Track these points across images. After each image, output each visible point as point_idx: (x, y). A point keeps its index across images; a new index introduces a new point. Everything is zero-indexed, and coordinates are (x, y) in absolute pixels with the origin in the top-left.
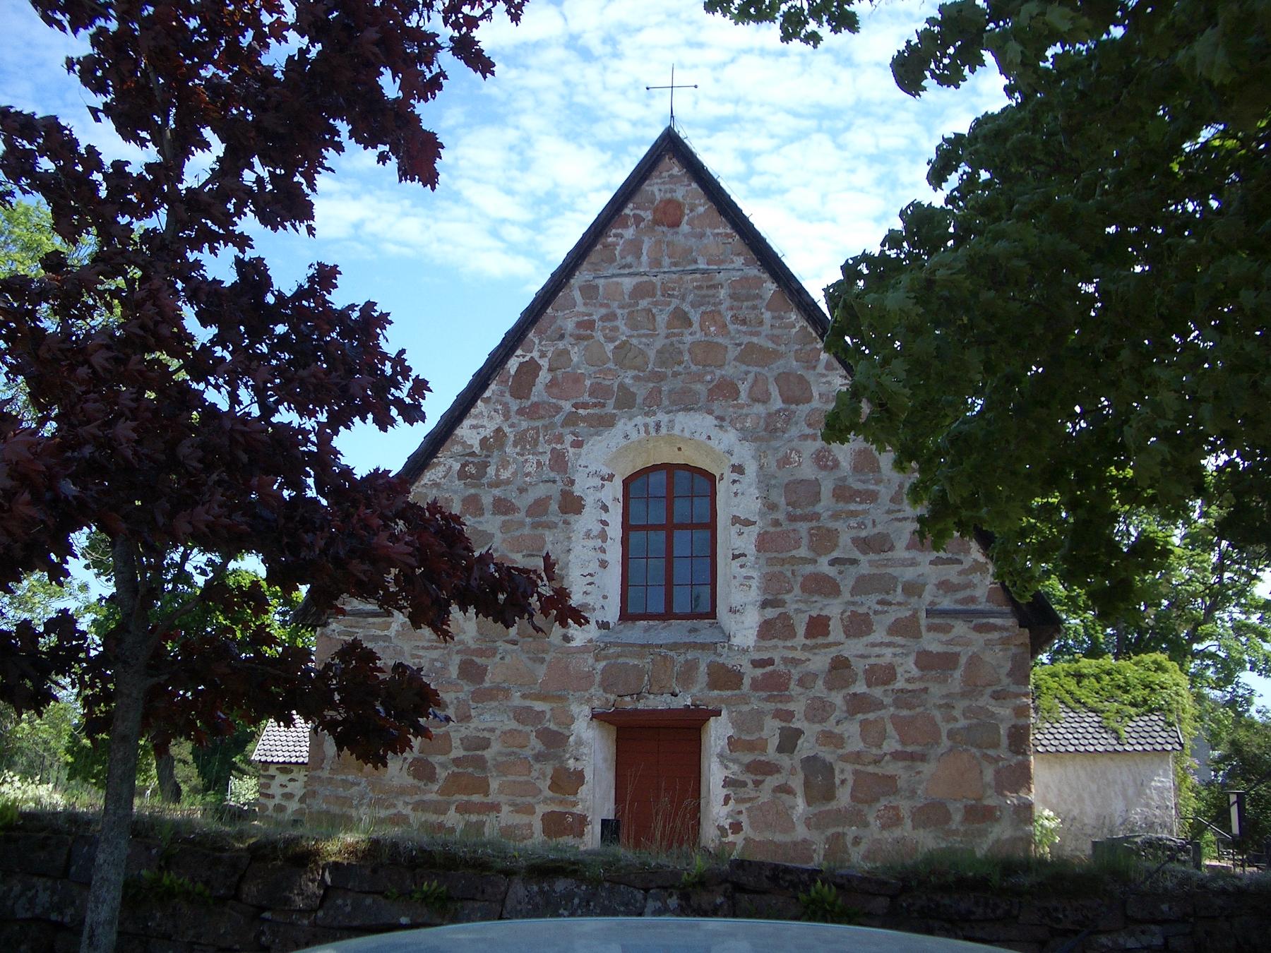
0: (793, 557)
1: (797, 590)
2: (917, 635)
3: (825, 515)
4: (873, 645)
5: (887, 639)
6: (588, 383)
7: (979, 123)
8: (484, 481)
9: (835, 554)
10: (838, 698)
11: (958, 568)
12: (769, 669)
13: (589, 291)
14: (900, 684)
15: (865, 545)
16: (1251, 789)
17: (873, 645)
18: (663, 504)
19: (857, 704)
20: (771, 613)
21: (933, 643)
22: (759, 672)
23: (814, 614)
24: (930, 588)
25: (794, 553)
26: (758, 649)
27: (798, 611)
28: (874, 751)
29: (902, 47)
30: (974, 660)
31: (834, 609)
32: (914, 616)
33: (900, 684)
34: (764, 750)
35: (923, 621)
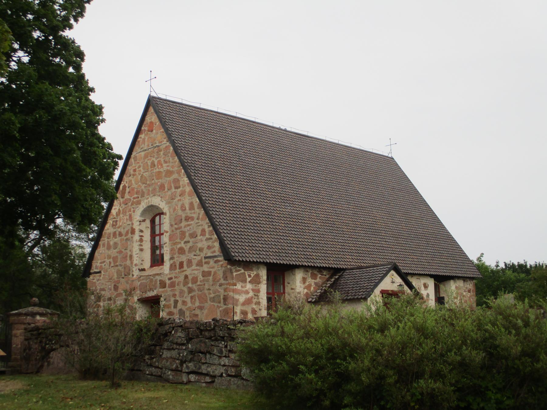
0: (176, 242)
1: (177, 254)
2: (202, 266)
3: (183, 227)
4: (193, 270)
5: (196, 268)
6: (135, 190)
7: (98, 110)
8: (117, 226)
9: (185, 240)
10: (185, 289)
11: (211, 241)
12: (172, 280)
13: (135, 158)
14: (199, 283)
15: (182, 238)
16: (509, 286)
17: (193, 270)
18: (159, 226)
19: (190, 290)
20: (172, 261)
21: (206, 268)
22: (170, 281)
23: (180, 261)
24: (205, 249)
25: (176, 241)
26: (170, 274)
27: (177, 260)
28: (194, 306)
29: (91, 85)
30: (215, 273)
31: (184, 258)
32: (201, 259)
33: (199, 283)
34: (171, 307)
35: (204, 261)
